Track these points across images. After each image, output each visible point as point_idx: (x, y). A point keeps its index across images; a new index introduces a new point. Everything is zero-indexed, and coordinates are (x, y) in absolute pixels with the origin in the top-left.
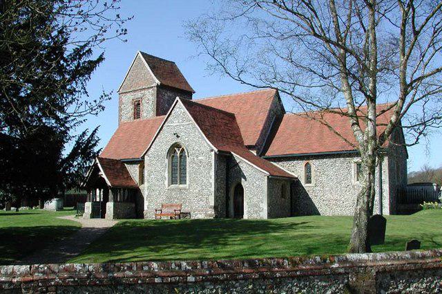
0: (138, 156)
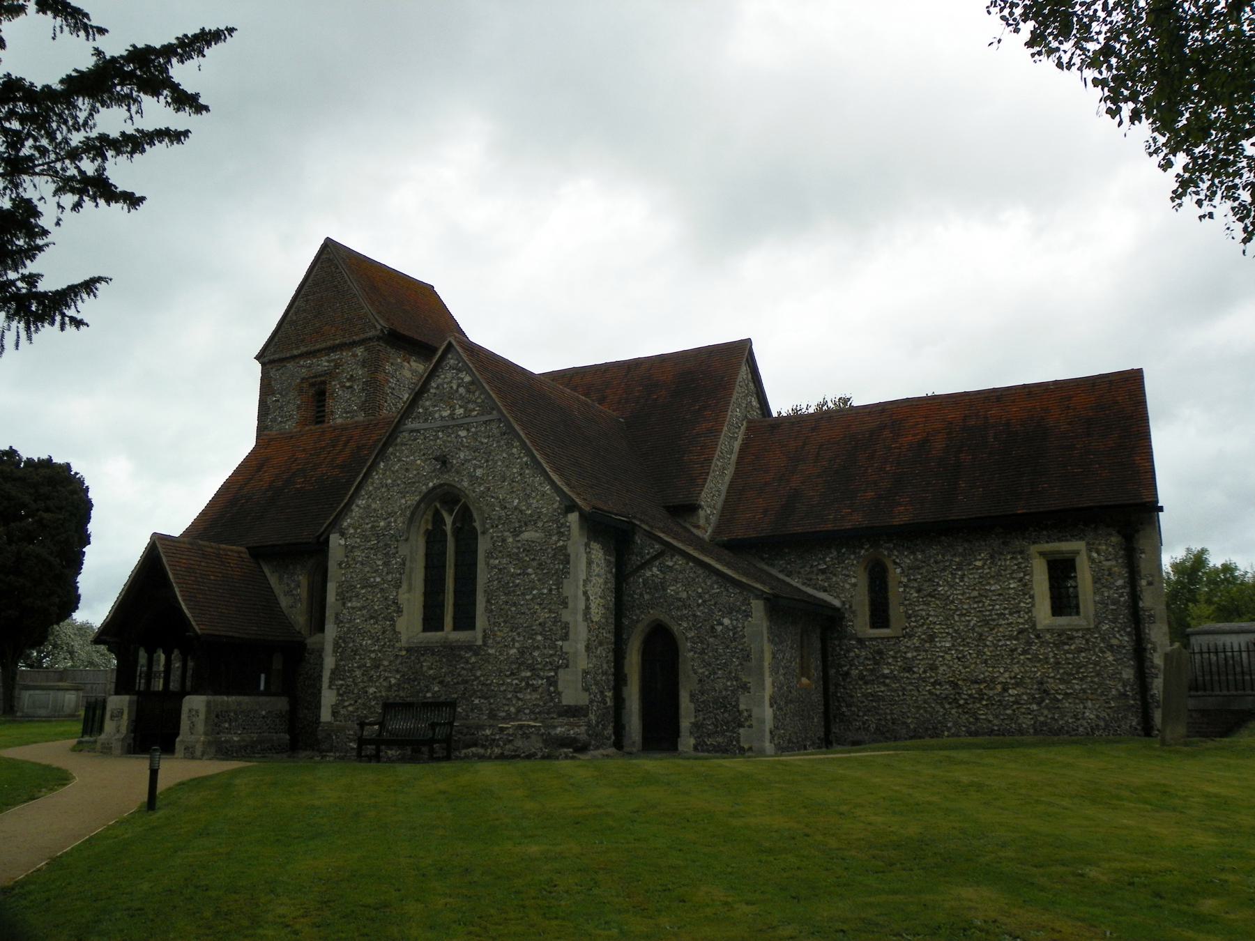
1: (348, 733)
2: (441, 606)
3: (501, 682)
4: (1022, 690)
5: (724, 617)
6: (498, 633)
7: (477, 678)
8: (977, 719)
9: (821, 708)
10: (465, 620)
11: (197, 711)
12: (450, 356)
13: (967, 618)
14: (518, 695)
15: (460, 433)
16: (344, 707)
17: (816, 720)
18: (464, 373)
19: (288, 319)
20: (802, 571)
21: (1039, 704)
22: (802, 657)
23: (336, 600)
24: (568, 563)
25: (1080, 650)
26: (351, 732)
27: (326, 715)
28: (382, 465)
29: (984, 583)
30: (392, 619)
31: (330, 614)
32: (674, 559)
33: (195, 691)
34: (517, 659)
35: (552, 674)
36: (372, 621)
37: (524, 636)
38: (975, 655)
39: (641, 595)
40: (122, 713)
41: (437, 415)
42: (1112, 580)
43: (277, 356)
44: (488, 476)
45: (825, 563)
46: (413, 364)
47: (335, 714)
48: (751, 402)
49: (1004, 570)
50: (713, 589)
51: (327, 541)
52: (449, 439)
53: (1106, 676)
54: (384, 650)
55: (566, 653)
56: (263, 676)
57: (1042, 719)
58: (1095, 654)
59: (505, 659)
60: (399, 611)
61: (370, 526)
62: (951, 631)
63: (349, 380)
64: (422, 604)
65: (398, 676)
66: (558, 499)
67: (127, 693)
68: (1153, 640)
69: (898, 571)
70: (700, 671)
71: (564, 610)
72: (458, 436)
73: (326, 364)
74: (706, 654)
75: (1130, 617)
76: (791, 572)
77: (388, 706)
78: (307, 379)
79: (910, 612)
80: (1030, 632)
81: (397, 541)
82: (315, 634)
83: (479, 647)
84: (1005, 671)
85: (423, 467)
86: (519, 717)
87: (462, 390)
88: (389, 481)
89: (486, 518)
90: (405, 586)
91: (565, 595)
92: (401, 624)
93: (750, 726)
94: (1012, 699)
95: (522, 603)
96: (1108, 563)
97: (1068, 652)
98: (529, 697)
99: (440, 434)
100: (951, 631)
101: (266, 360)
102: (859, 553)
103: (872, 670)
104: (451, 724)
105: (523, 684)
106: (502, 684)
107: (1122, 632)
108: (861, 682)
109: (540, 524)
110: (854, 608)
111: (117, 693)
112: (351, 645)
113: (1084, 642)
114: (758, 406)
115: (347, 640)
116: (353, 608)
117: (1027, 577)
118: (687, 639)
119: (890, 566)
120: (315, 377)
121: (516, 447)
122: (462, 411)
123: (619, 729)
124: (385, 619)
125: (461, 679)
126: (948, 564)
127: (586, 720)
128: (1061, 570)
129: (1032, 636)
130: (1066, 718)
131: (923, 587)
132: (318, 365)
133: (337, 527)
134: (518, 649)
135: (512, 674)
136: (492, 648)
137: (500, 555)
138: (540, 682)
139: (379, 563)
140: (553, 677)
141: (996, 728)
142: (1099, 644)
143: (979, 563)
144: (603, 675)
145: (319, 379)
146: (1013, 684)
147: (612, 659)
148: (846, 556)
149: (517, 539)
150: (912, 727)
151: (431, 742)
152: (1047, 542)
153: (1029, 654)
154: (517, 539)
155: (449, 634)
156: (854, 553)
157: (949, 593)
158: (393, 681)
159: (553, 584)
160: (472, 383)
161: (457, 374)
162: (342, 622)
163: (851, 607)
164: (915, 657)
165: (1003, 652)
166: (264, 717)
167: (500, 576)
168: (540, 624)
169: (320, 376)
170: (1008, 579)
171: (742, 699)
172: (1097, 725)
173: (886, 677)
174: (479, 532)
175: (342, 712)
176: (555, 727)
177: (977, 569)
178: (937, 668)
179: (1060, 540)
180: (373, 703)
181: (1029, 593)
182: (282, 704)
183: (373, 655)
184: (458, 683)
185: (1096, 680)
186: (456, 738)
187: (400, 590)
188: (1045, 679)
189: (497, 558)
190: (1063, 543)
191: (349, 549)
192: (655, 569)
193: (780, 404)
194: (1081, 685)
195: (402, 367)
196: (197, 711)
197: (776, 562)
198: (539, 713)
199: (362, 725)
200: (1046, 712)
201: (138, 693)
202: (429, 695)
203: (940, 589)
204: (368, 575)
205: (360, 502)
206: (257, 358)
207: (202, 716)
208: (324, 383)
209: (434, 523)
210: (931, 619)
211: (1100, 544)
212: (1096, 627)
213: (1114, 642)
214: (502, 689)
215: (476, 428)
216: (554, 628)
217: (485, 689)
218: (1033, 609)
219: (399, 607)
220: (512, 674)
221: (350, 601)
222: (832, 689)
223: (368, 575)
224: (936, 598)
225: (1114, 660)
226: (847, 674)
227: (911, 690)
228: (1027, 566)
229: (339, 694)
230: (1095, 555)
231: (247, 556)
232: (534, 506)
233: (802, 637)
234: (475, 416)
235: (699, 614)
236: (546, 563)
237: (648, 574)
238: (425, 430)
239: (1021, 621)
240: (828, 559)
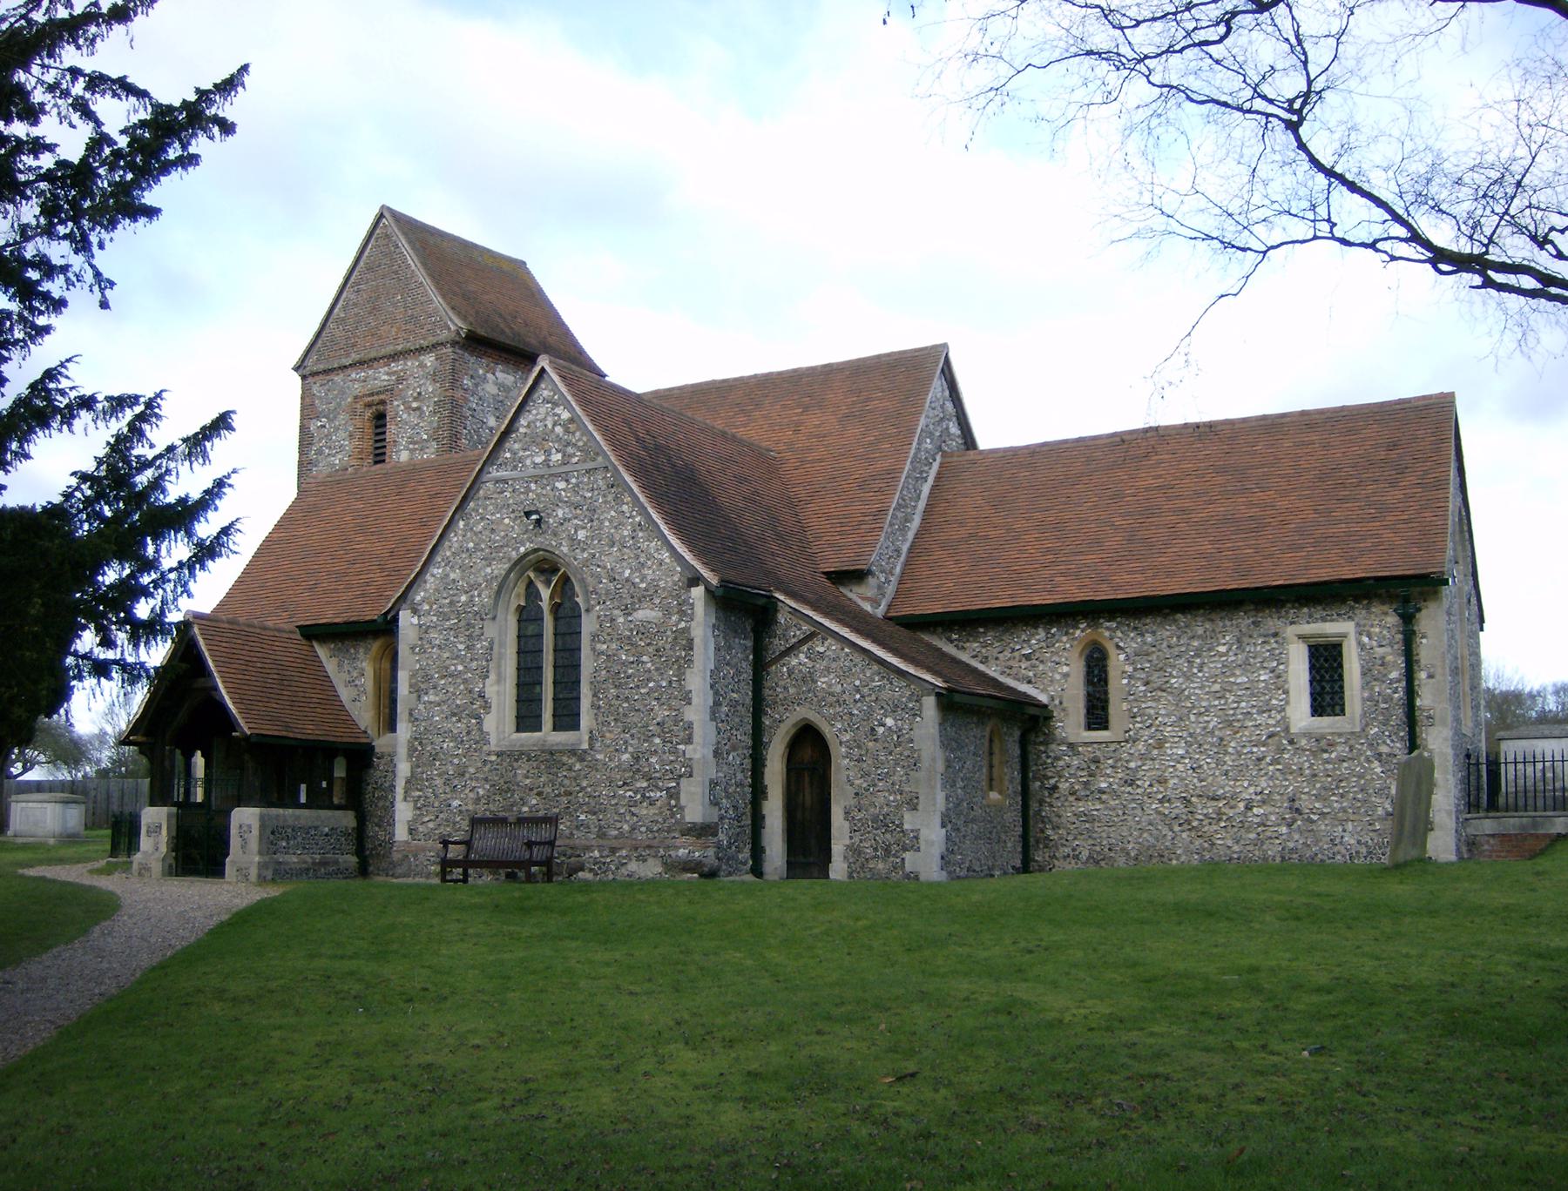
0: (372, 613)
1: (428, 853)
4: (1271, 809)
5: (886, 717)
6: (608, 735)
7: (583, 789)
8: (1213, 844)
9: (1019, 830)
10: (567, 717)
11: (249, 826)
12: (543, 386)
13: (1206, 718)
14: (633, 809)
15: (557, 484)
17: (1009, 845)
18: (562, 407)
19: (334, 315)
20: (1000, 656)
21: (1289, 826)
22: (991, 766)
23: (410, 692)
24: (692, 649)
27: (401, 834)
28: (461, 524)
29: (1227, 674)
30: (478, 717)
31: (401, 709)
32: (826, 644)
33: (240, 803)
36: (454, 719)
37: (639, 738)
38: (1214, 765)
39: (785, 688)
40: (160, 827)
42: (1385, 672)
43: (321, 367)
44: (592, 540)
45: (1030, 647)
46: (498, 374)
47: (411, 831)
48: (947, 428)
49: (1254, 658)
50: (874, 681)
51: (395, 619)
53: (1371, 791)
55: (690, 759)
56: (303, 787)
57: (1291, 845)
58: (1360, 764)
59: (617, 766)
60: (487, 706)
61: (447, 601)
62: (1185, 734)
63: (415, 399)
64: (514, 713)
66: (679, 569)
67: (164, 805)
68: (1431, 747)
69: (1122, 657)
70: (857, 782)
73: (386, 377)
75: (1404, 719)
76: (987, 657)
77: (475, 822)
78: (361, 397)
79: (1135, 710)
80: (1283, 736)
81: (482, 619)
82: (384, 734)
83: (585, 751)
84: (1250, 785)
85: (513, 527)
87: (558, 429)
88: (471, 545)
90: (493, 677)
91: (687, 688)
92: (490, 723)
94: (1256, 820)
95: (636, 697)
96: (1380, 651)
97: (1327, 761)
99: (533, 486)
100: (1185, 734)
101: (306, 372)
102: (1073, 634)
103: (1086, 783)
104: (551, 844)
105: (639, 796)
106: (614, 796)
107: (1393, 737)
108: (1071, 798)
109: (657, 601)
110: (1065, 704)
111: (152, 804)
113: (1347, 749)
114: (959, 432)
115: (424, 741)
116: (431, 703)
117: (1281, 667)
118: (841, 743)
119: (1112, 651)
120: (372, 394)
121: (627, 504)
122: (559, 456)
123: (758, 852)
125: (563, 789)
126: (1183, 649)
127: (715, 840)
128: (1326, 660)
129: (1285, 742)
130: (1321, 844)
131: (1152, 679)
132: (376, 379)
133: (409, 602)
136: (600, 752)
138: (659, 794)
139: (461, 647)
141: (1235, 856)
142: (1365, 751)
143: (1222, 649)
144: (737, 786)
145: (376, 398)
146: (1258, 801)
147: (749, 767)
148: (1057, 637)
149: (630, 618)
150: (1133, 854)
151: (525, 864)
152: (1308, 623)
153: (1279, 764)
154: (630, 618)
155: (548, 735)
156: (1067, 634)
157: (1184, 686)
158: (481, 792)
159: (674, 675)
160: (571, 420)
161: (553, 409)
162: (417, 719)
163: (1061, 703)
164: (1140, 767)
165: (1249, 762)
166: (327, 835)
168: (658, 724)
169: (378, 393)
170: (1259, 669)
172: (1357, 852)
173: (1102, 792)
174: (583, 611)
175: (421, 830)
176: (677, 848)
177: (1221, 656)
178: (1166, 781)
179: (1324, 620)
180: (458, 819)
181: (1283, 687)
182: (347, 819)
183: (456, 761)
184: (559, 795)
185: (1360, 796)
186: (559, 861)
188: (1298, 796)
189: (604, 643)
190: (1327, 624)
191: (424, 629)
192: (802, 656)
193: (991, 434)
194: (1341, 803)
195: (485, 380)
196: (249, 826)
197: (968, 644)
198: (657, 831)
199: (445, 843)
200: (1296, 836)
201: (177, 805)
202: (525, 809)
203: (1173, 681)
204: (448, 662)
205: (435, 571)
206: (296, 369)
207: (255, 832)
208: (383, 402)
209: (528, 596)
210: (1160, 719)
211: (1372, 626)
213: (1384, 749)
218: (1288, 708)
219: (486, 702)
221: (426, 693)
222: (1034, 806)
223: (448, 662)
224: (1168, 693)
225: (1382, 772)
226: (1055, 788)
227: (1133, 808)
228: (1281, 653)
230: (1365, 639)
231: (299, 637)
232: (649, 578)
233: (991, 741)
235: (856, 712)
237: (794, 662)
239: (1271, 722)
240: (1034, 642)
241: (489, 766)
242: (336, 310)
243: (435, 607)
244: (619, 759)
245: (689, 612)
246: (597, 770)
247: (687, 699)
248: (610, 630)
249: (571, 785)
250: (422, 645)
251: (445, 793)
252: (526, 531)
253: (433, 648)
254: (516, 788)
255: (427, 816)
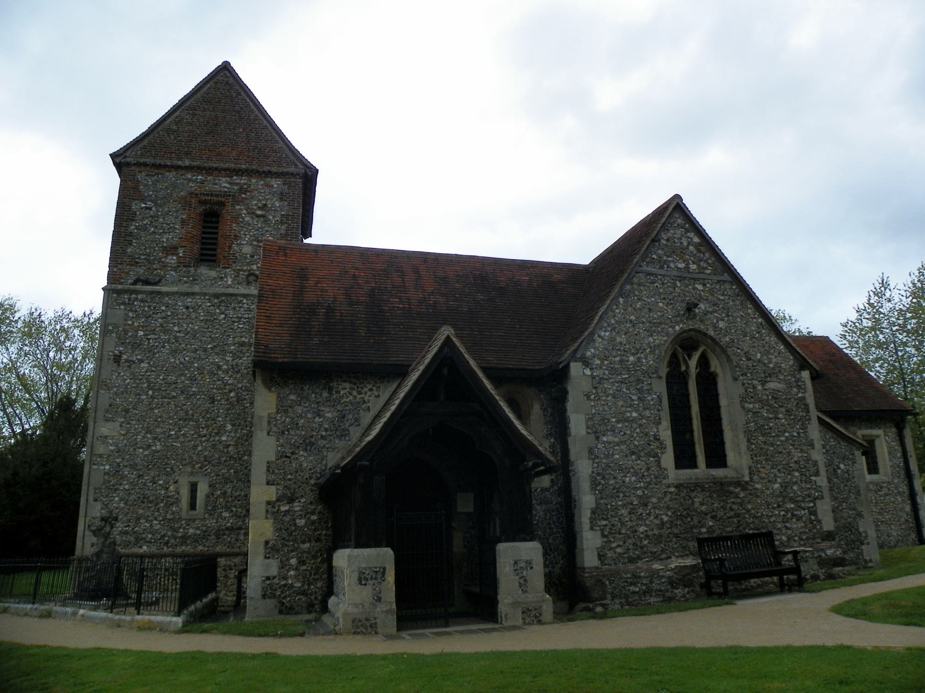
2: (692, 444)
3: (770, 514)
7: (748, 511)
10: (717, 457)
14: (787, 524)
16: (611, 549)
23: (588, 433)
25: (886, 495)
26: (629, 575)
34: (781, 492)
35: (812, 505)
36: (634, 457)
41: (672, 265)
47: (601, 557)
52: (687, 289)
54: (651, 486)
61: (618, 359)
65: (670, 513)
71: (812, 450)
72: (695, 288)
73: (227, 185)
74: (834, 490)
81: (650, 377)
83: (746, 483)
86: (791, 544)
89: (736, 367)
93: (868, 544)
98: (795, 526)
112: (612, 482)
116: (609, 443)
124: (649, 455)
134: (780, 483)
135: (779, 506)
136: (758, 483)
137: (753, 400)
138: (803, 512)
140: (812, 507)
161: (686, 233)
167: (756, 419)
171: (860, 523)
175: (609, 555)
179: (871, 428)
185: (894, 512)
187: (660, 426)
191: (597, 382)
196: (529, 563)
198: (806, 539)
202: (704, 530)
204: (624, 409)
208: (222, 204)
212: (892, 481)
213: (901, 490)
214: (772, 520)
215: (711, 285)
216: (807, 465)
217: (757, 521)
219: (661, 444)
220: (779, 506)
221: (604, 435)
223: (624, 409)
229: (603, 536)
230: (887, 438)
234: (709, 274)
236: (792, 410)
238: (663, 276)
241: (669, 496)
242: (168, 122)
243: (606, 362)
244: (772, 488)
245: (803, 387)
246: (757, 496)
247: (811, 445)
248: (752, 394)
249: (738, 509)
250: (597, 393)
251: (631, 521)
252: (678, 315)
253: (607, 396)
254: (694, 513)
255: (614, 542)
